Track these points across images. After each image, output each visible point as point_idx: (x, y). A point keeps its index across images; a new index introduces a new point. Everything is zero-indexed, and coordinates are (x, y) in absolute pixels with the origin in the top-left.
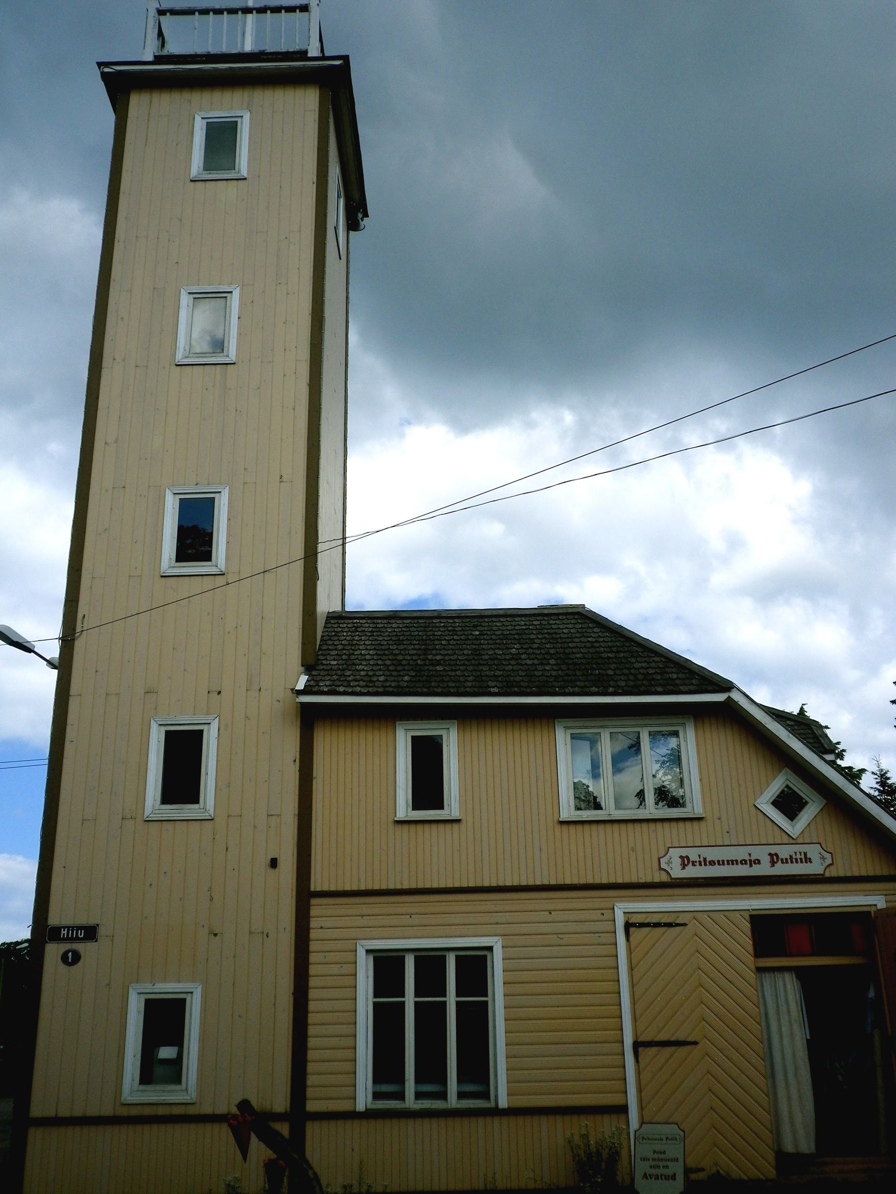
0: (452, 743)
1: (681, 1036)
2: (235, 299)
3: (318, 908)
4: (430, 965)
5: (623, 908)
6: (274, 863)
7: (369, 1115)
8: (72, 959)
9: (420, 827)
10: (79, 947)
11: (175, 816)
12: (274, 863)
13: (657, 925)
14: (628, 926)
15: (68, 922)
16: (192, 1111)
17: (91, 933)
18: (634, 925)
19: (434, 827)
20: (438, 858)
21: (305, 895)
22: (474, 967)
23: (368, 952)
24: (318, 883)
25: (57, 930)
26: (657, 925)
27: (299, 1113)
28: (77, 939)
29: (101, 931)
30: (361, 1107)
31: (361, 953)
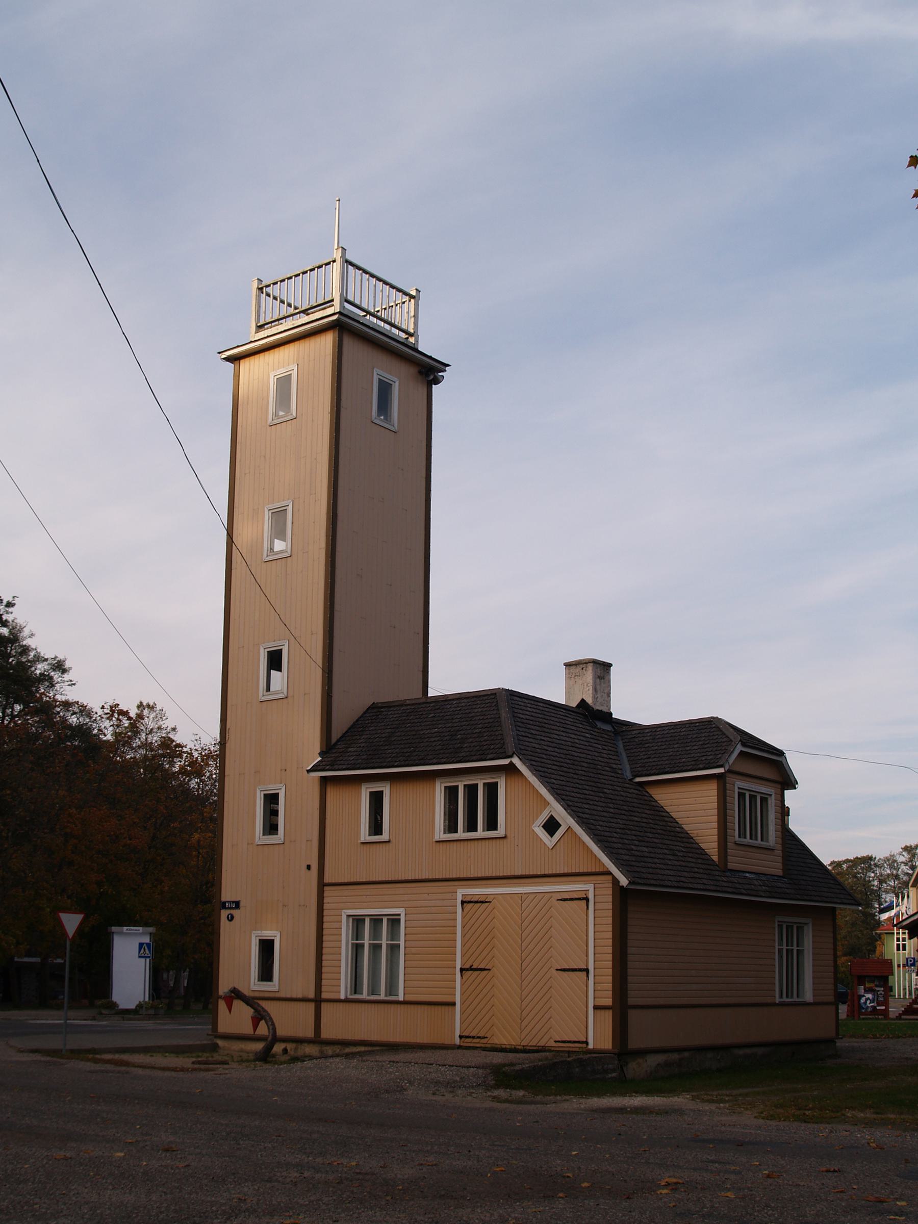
0: (386, 789)
1: (482, 966)
2: (458, 1033)
3: (328, 891)
4: (376, 921)
5: (462, 892)
6: (309, 867)
7: (347, 1001)
8: (231, 918)
9: (483, 842)
10: (233, 912)
11: (268, 842)
12: (309, 867)
13: (477, 902)
14: (463, 902)
15: (228, 899)
16: (277, 995)
17: (237, 905)
18: (465, 902)
19: (473, 842)
20: (380, 865)
21: (322, 885)
22: (394, 922)
23: (349, 916)
24: (327, 880)
25: (224, 903)
26: (477, 902)
27: (318, 1001)
28: (231, 908)
29: (241, 904)
30: (342, 997)
31: (344, 918)
